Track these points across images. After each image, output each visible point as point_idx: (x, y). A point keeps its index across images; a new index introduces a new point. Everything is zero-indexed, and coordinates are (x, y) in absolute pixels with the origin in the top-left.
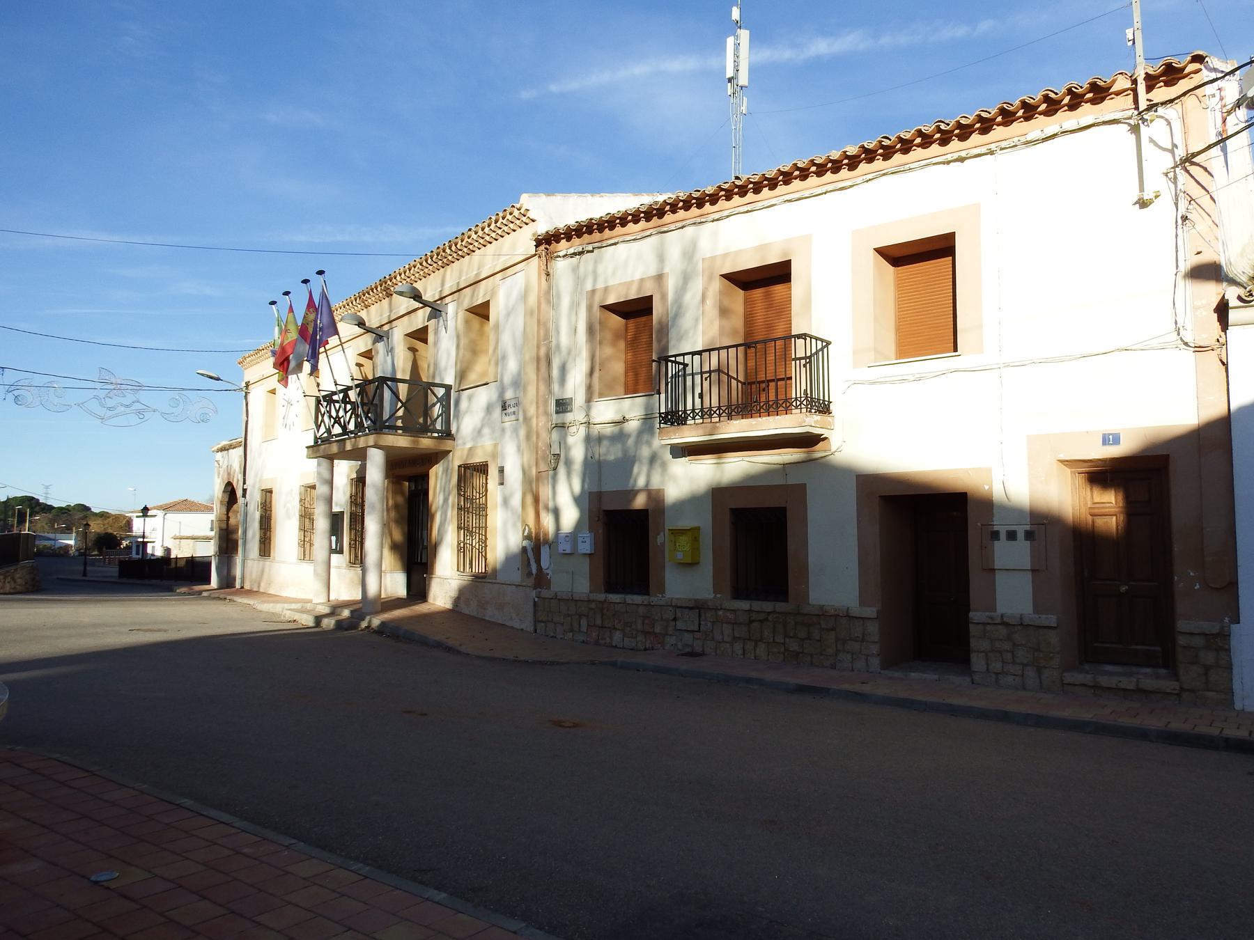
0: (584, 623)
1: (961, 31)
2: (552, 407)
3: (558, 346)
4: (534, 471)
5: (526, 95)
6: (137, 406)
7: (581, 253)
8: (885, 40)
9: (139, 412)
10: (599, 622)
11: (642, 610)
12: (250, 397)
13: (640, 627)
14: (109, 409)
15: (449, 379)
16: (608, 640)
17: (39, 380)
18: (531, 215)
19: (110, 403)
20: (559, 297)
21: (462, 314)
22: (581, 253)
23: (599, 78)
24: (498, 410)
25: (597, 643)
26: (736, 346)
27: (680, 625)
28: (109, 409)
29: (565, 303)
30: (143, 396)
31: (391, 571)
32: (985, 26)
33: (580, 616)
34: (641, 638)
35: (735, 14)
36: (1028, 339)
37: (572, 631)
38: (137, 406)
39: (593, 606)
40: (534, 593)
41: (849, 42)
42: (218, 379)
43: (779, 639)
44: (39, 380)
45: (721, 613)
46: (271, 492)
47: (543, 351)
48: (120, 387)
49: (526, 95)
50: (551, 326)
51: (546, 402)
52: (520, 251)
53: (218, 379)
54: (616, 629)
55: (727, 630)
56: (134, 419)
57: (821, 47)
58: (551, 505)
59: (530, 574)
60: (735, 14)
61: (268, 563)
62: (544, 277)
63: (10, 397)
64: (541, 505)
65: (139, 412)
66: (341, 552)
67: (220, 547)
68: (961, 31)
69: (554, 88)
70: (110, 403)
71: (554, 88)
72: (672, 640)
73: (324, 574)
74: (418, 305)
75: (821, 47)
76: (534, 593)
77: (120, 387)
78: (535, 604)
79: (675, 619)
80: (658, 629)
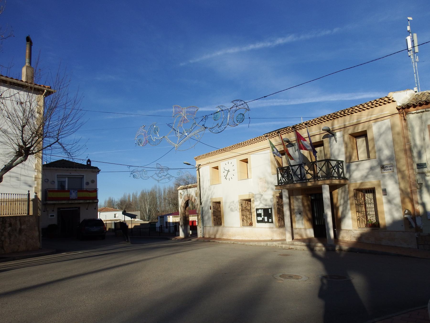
1: (328, 32)
2: (415, 166)
3: (415, 145)
4: (409, 190)
5: (182, 64)
6: (168, 176)
7: (423, 112)
8: (302, 37)
9: (169, 178)
12: (200, 170)
14: (160, 177)
15: (342, 158)
17: (140, 169)
18: (394, 99)
19: (160, 175)
20: (412, 127)
21: (347, 137)
22: (423, 112)
23: (206, 57)
24: (378, 170)
28: (160, 177)
29: (417, 130)
30: (170, 172)
31: (309, 228)
32: (336, 30)
35: (409, 28)
38: (168, 176)
40: (416, 234)
41: (290, 38)
42: (190, 164)
44: (140, 169)
46: (219, 203)
47: (407, 147)
48: (162, 169)
49: (182, 64)
50: (410, 138)
51: (412, 165)
52: (388, 112)
53: (190, 164)
56: (167, 180)
57: (280, 41)
58: (420, 201)
59: (412, 227)
60: (409, 28)
61: (220, 228)
62: (403, 121)
63: (132, 175)
64: (414, 202)
65: (169, 178)
67: (184, 223)
68: (328, 32)
69: (191, 61)
70: (160, 175)
71: (191, 61)
75: (280, 41)
76: (416, 234)
77: (162, 169)
78: (417, 238)
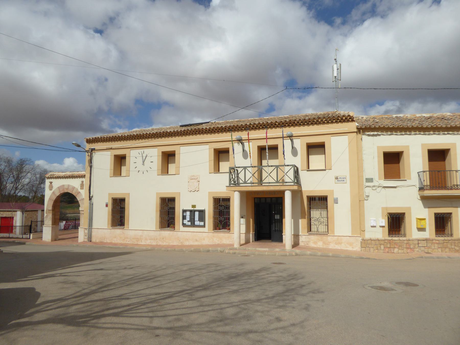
0: (382, 247)
10: (389, 246)
11: (405, 242)
13: (405, 246)
16: (392, 251)
25: (388, 252)
26: (424, 172)
27: (420, 245)
33: (381, 244)
34: (405, 250)
36: (3, 133)
37: (377, 249)
39: (386, 241)
43: (453, 247)
45: (434, 241)
54: (395, 248)
55: (436, 245)
66: (184, 211)
72: (417, 249)
73: (130, 149)
74: (15, 178)
79: (418, 244)
80: (412, 247)
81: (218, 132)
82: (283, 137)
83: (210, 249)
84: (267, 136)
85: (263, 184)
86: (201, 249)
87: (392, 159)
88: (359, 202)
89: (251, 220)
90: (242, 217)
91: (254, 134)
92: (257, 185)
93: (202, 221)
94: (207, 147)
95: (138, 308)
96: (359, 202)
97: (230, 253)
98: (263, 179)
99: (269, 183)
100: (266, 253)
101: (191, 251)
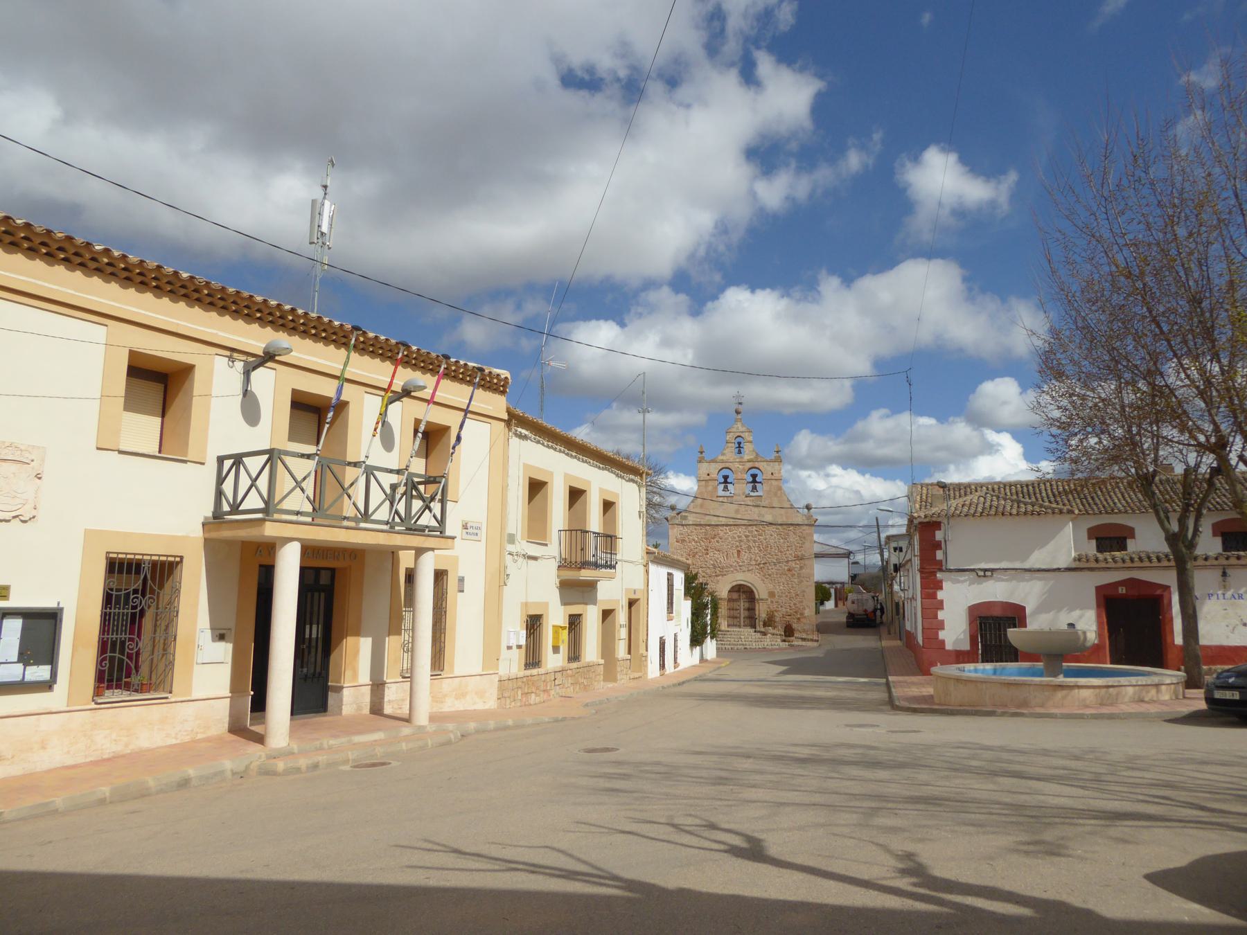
81: (159, 290)
82: (466, 411)
83: (191, 772)
84: (343, 370)
85: (276, 516)
86: (151, 783)
87: (157, 383)
88: (499, 579)
89: (1179, 640)
90: (222, 637)
91: (304, 350)
92: (309, 519)
93: (38, 663)
94: (97, 332)
95: (595, 872)
96: (499, 579)
97: (298, 770)
98: (277, 500)
99: (298, 513)
100: (404, 746)
101: (102, 802)
